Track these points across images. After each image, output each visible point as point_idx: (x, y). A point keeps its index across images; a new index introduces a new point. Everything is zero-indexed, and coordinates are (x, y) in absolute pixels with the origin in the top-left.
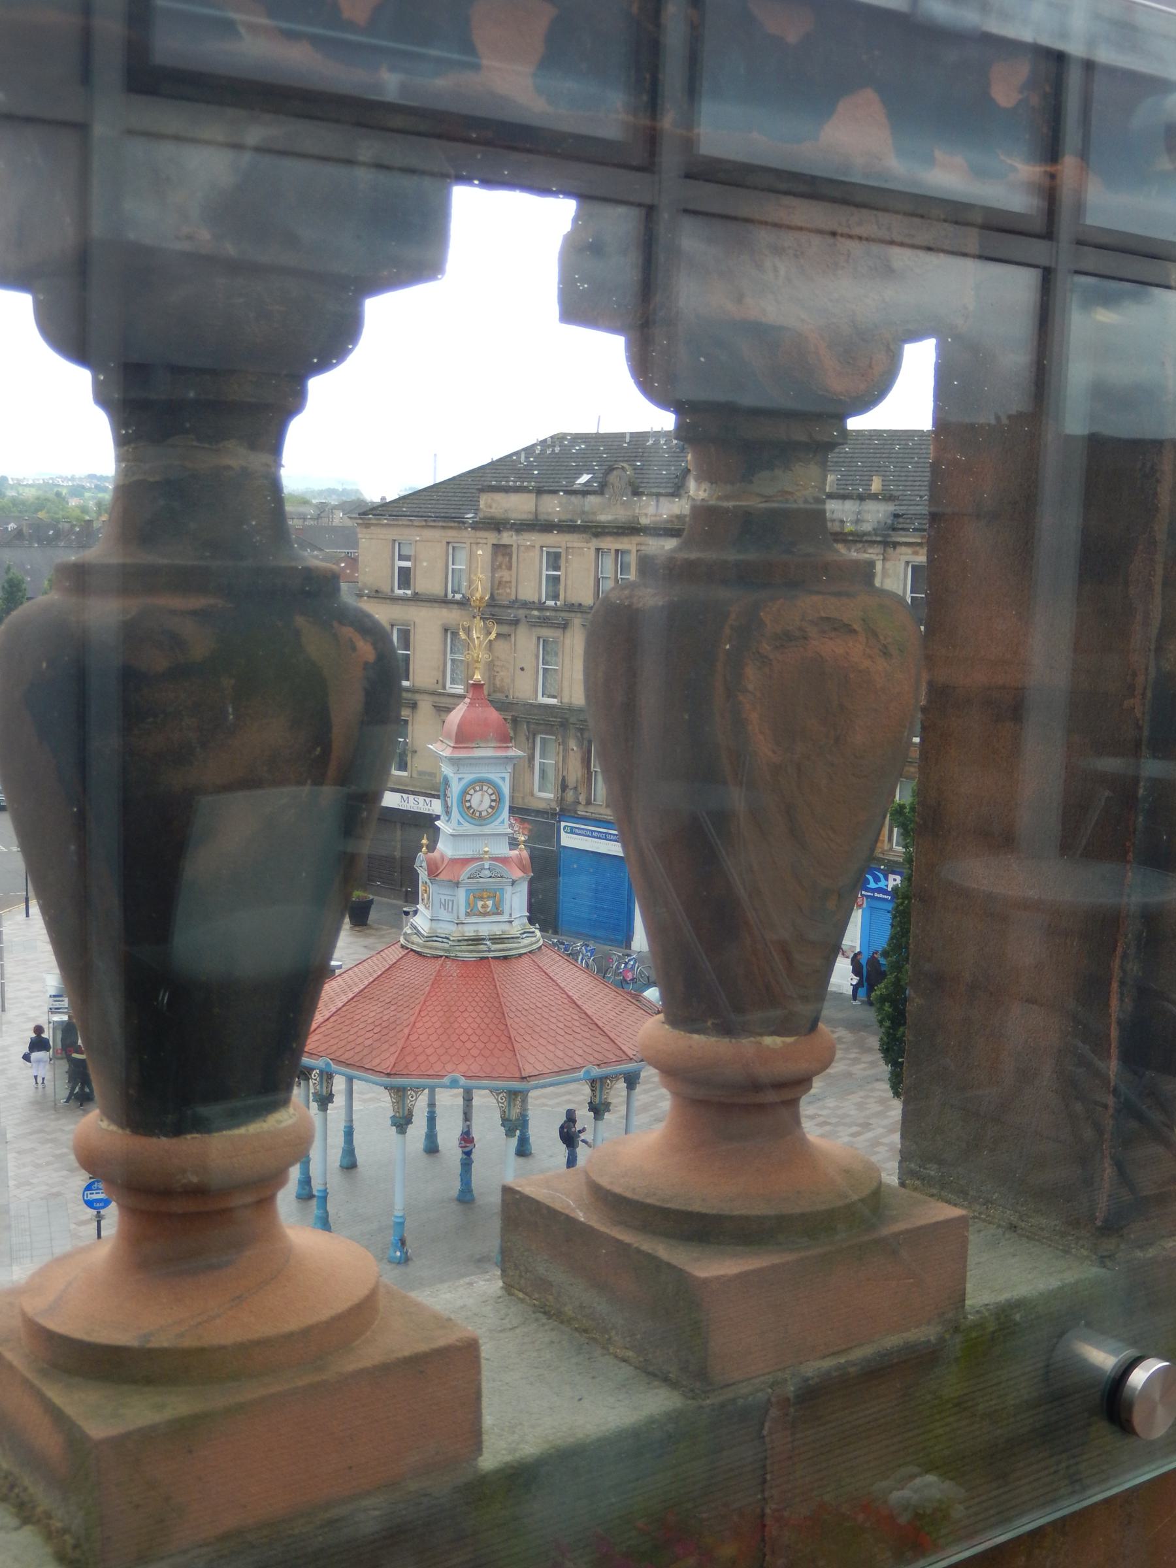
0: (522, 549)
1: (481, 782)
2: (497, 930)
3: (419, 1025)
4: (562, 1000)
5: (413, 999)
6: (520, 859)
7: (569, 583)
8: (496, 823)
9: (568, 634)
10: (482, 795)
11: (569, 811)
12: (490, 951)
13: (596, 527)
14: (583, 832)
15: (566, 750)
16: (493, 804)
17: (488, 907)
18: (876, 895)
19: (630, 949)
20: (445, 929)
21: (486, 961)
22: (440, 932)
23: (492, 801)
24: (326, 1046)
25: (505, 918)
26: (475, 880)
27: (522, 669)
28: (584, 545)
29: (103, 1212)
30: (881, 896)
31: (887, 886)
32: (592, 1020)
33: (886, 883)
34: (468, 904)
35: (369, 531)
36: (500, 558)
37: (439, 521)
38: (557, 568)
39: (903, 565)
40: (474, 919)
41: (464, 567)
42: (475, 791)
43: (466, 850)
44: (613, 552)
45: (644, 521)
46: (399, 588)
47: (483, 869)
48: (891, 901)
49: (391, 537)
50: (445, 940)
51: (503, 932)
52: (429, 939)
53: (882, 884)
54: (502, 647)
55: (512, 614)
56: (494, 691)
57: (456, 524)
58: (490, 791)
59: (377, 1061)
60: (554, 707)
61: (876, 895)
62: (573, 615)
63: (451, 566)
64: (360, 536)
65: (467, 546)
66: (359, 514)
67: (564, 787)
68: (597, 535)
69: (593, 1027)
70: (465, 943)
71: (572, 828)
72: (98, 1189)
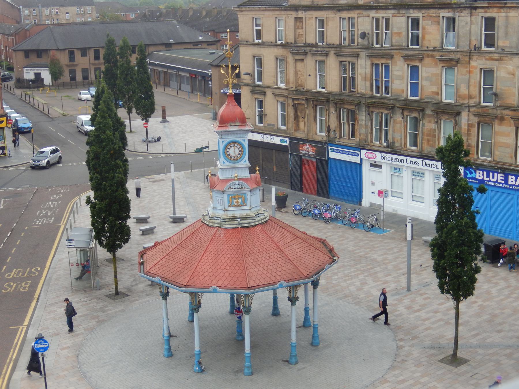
0: (307, 19)
1: (234, 143)
2: (244, 213)
3: (202, 261)
4: (274, 247)
5: (201, 248)
6: (256, 178)
7: (328, 34)
9: (329, 58)
10: (235, 149)
11: (332, 141)
12: (239, 224)
13: (339, 7)
14: (338, 151)
15: (330, 113)
16: (240, 153)
18: (471, 180)
19: (361, 205)
20: (220, 213)
21: (237, 229)
23: (240, 151)
24: (161, 270)
25: (248, 207)
26: (231, 190)
27: (310, 75)
28: (334, 15)
29: (44, 353)
30: (473, 181)
31: (476, 176)
32: (288, 257)
33: (475, 175)
34: (229, 201)
35: (242, 13)
36: (298, 24)
37: (271, 7)
38: (323, 28)
39: (480, 17)
41: (283, 29)
42: (231, 147)
43: (227, 175)
44: (347, 18)
46: (257, 40)
48: (478, 183)
49: (252, 16)
50: (219, 219)
51: (247, 215)
52: (213, 218)
53: (473, 175)
54: (299, 65)
55: (303, 50)
56: (298, 86)
57: (278, 9)
59: (181, 279)
60: (324, 93)
61: (471, 180)
62: (330, 49)
63: (278, 29)
64: (239, 16)
65: (284, 18)
66: (238, 6)
67: (329, 130)
68: (339, 10)
69: (288, 261)
70: (228, 220)
71: (333, 149)
72: (41, 343)
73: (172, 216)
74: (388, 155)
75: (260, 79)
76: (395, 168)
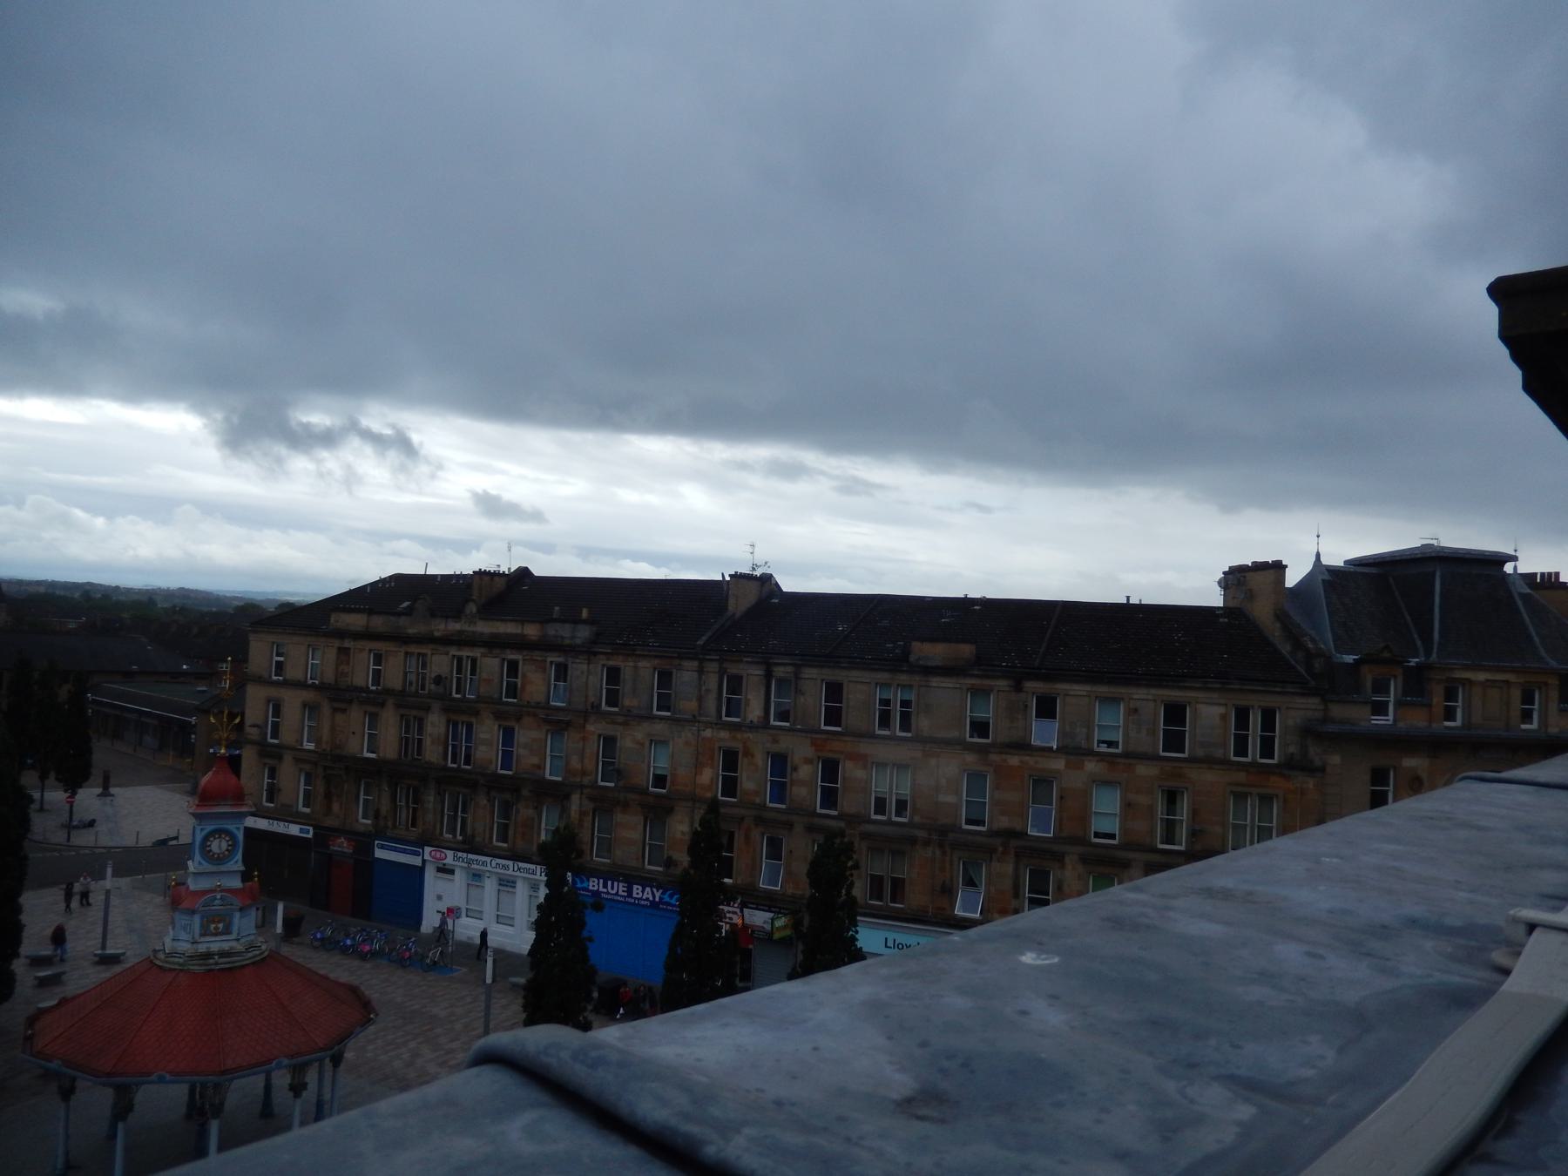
2: (226, 946)
8: (232, 862)
12: (217, 964)
17: (219, 929)
20: (184, 947)
22: (180, 949)
23: (229, 845)
25: (234, 936)
26: (208, 908)
27: (354, 733)
34: (202, 926)
39: (600, 668)
40: (208, 939)
45: (437, 634)
47: (216, 899)
51: (231, 948)
52: (170, 955)
53: (585, 885)
54: (339, 717)
58: (227, 838)
63: (310, 662)
64: (250, 639)
73: (99, 952)
74: (465, 855)
75: (275, 735)
76: (475, 875)
